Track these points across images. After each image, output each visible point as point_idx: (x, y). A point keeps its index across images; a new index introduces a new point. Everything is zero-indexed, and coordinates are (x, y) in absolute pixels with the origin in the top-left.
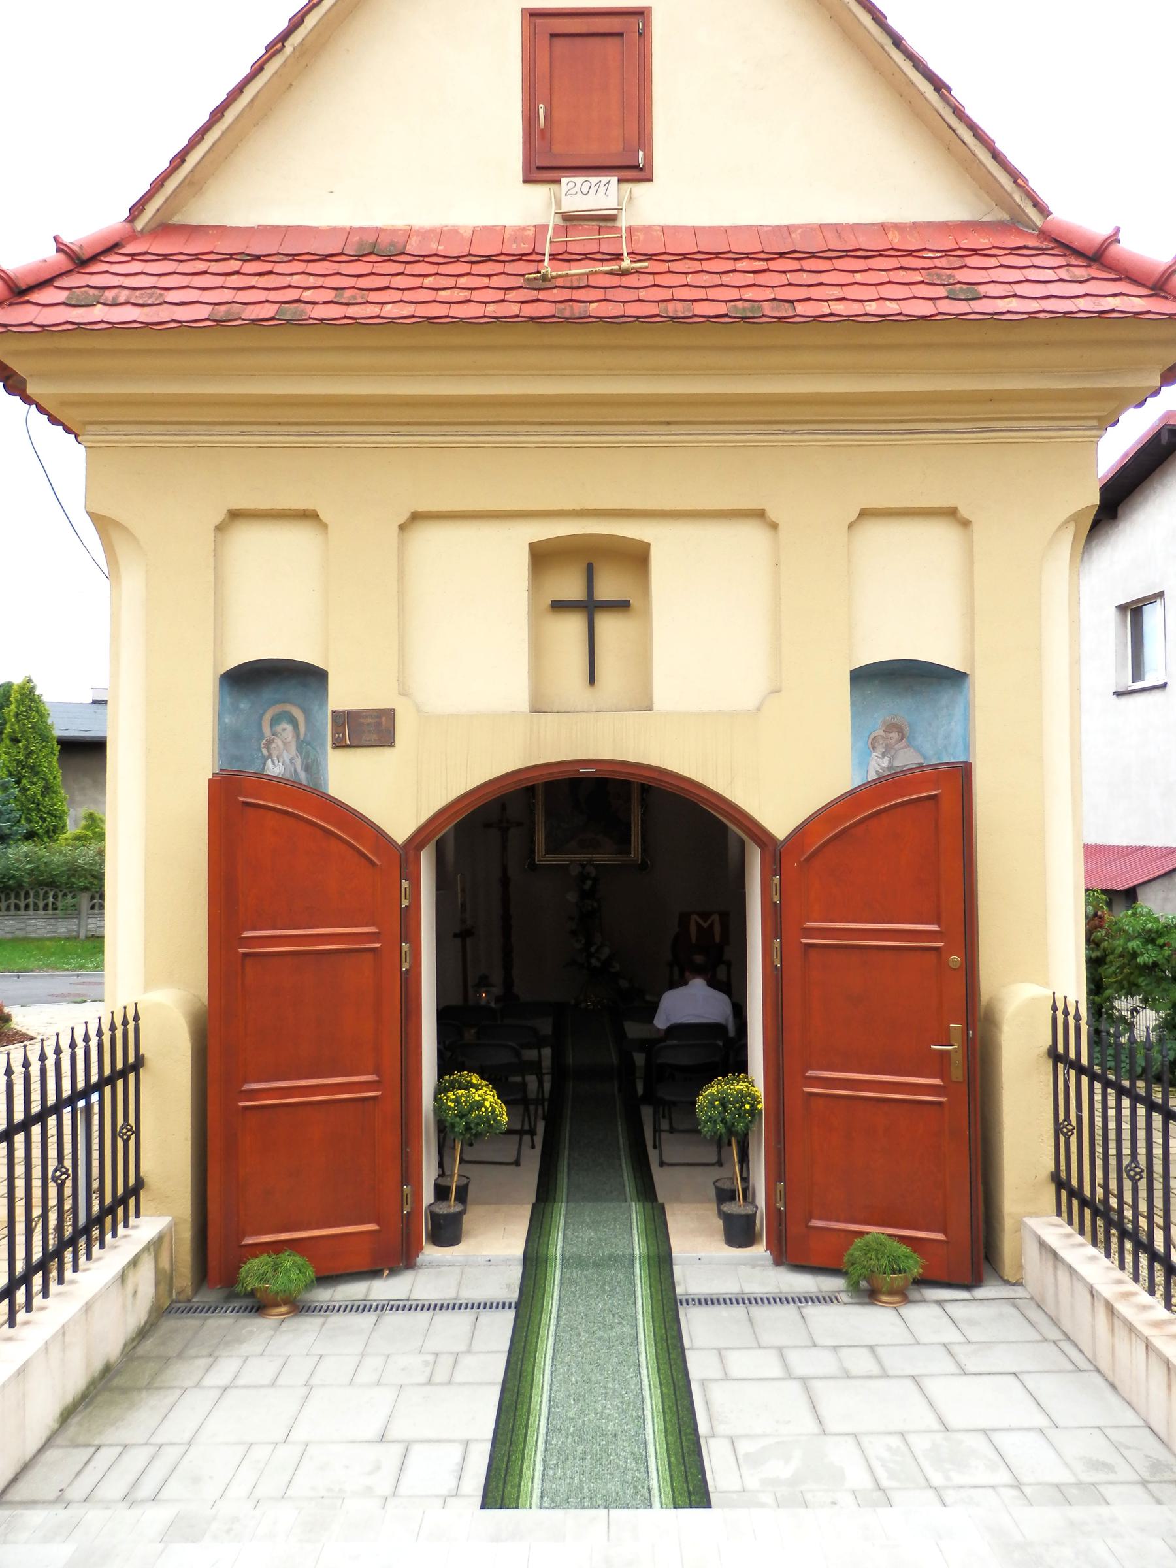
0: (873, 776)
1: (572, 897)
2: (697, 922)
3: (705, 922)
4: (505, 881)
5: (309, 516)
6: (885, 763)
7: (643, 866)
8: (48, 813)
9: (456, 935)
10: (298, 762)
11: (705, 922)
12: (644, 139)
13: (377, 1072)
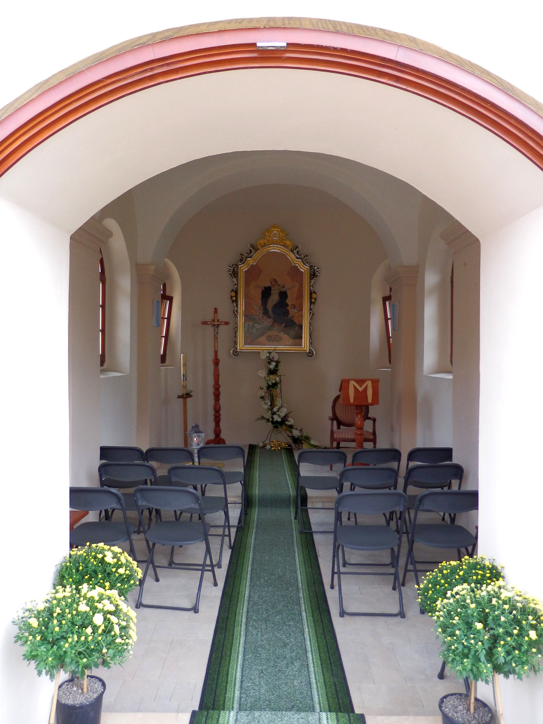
1: (263, 373)
2: (355, 387)
3: (361, 386)
4: (216, 362)
7: (310, 354)
9: (179, 397)
11: (361, 386)
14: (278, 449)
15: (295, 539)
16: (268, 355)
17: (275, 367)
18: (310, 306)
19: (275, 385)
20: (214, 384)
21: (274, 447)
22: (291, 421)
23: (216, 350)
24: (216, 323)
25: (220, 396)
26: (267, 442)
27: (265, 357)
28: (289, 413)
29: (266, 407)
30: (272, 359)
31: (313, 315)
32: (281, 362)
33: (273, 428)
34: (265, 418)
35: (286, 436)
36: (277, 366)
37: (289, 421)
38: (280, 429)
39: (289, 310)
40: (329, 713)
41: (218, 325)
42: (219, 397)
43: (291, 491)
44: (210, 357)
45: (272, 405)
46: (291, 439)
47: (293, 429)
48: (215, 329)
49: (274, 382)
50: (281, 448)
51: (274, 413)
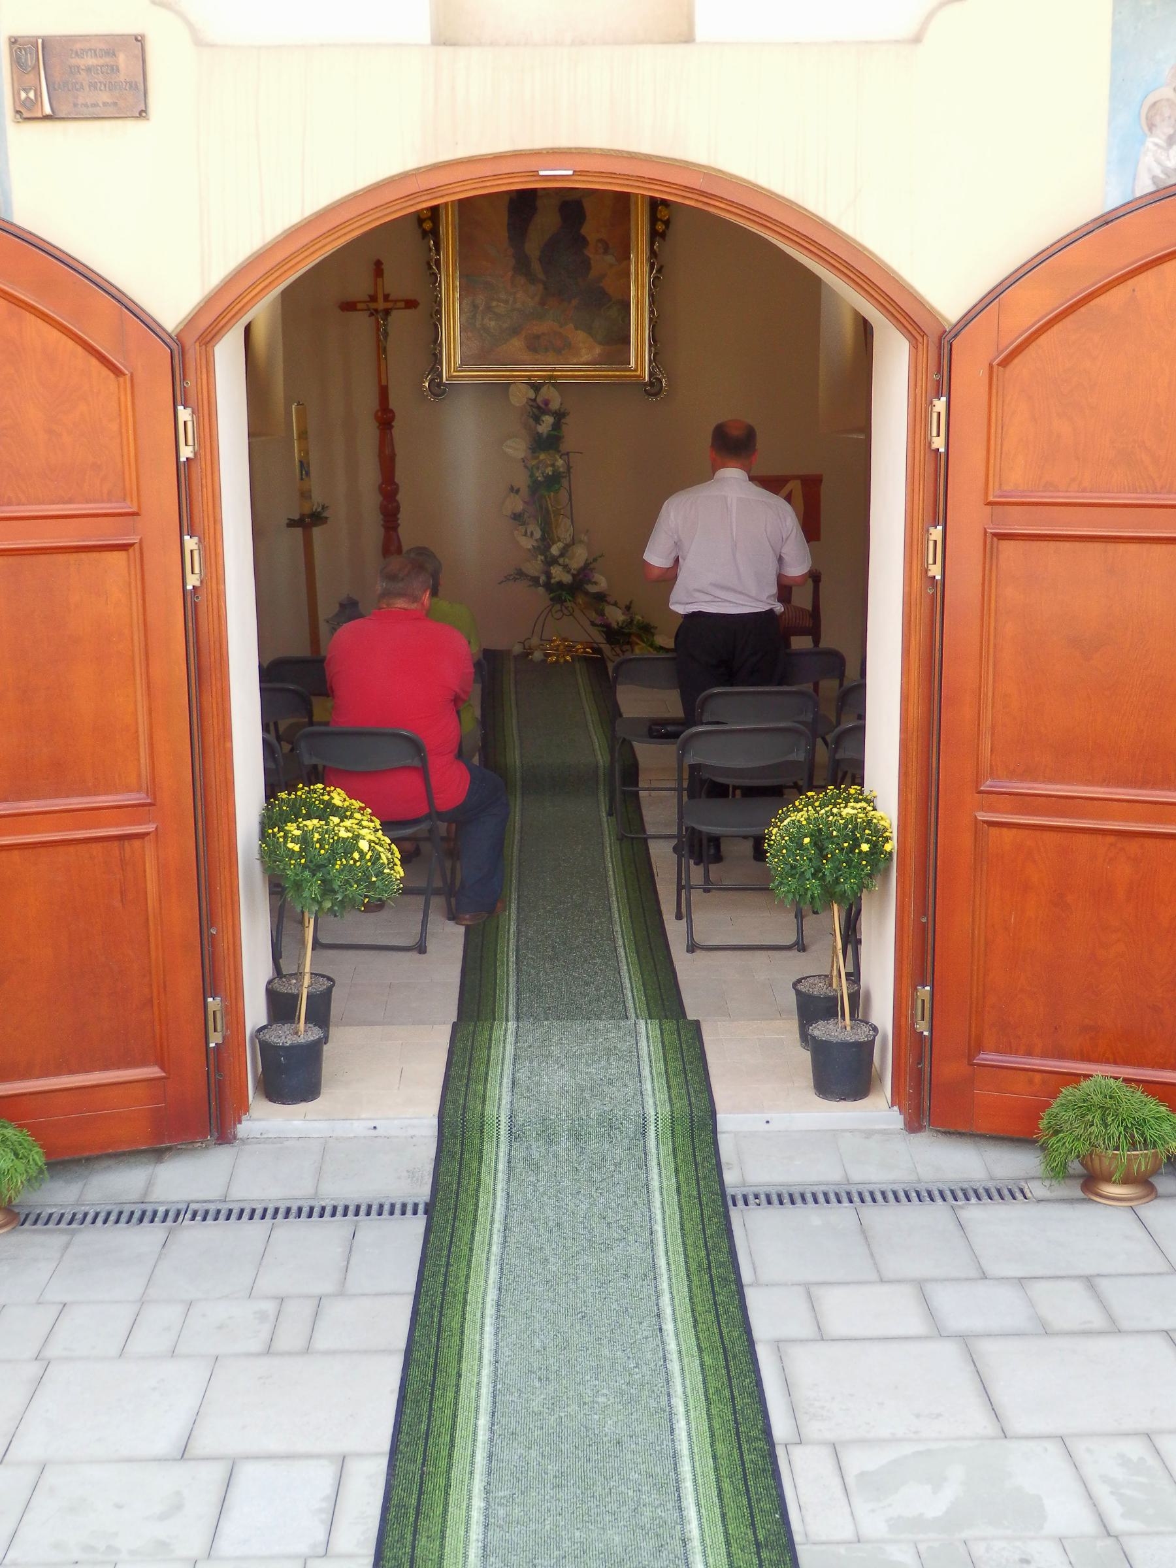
7: (653, 388)
9: (292, 523)
14: (566, 661)
15: (608, 849)
16: (532, 394)
17: (553, 429)
18: (652, 244)
19: (553, 480)
20: (380, 481)
21: (554, 654)
22: (601, 583)
23: (384, 383)
24: (381, 305)
25: (399, 516)
26: (535, 641)
27: (525, 400)
28: (595, 560)
29: (527, 543)
30: (543, 406)
31: (659, 271)
32: (568, 414)
33: (550, 603)
34: (527, 576)
35: (587, 624)
36: (557, 426)
37: (596, 583)
38: (569, 604)
39: (591, 256)
40: (649, 1021)
41: (387, 312)
42: (398, 519)
43: (600, 757)
44: (367, 403)
45: (547, 540)
46: (599, 631)
47: (604, 603)
48: (378, 322)
49: (549, 471)
50: (572, 657)
51: (552, 561)
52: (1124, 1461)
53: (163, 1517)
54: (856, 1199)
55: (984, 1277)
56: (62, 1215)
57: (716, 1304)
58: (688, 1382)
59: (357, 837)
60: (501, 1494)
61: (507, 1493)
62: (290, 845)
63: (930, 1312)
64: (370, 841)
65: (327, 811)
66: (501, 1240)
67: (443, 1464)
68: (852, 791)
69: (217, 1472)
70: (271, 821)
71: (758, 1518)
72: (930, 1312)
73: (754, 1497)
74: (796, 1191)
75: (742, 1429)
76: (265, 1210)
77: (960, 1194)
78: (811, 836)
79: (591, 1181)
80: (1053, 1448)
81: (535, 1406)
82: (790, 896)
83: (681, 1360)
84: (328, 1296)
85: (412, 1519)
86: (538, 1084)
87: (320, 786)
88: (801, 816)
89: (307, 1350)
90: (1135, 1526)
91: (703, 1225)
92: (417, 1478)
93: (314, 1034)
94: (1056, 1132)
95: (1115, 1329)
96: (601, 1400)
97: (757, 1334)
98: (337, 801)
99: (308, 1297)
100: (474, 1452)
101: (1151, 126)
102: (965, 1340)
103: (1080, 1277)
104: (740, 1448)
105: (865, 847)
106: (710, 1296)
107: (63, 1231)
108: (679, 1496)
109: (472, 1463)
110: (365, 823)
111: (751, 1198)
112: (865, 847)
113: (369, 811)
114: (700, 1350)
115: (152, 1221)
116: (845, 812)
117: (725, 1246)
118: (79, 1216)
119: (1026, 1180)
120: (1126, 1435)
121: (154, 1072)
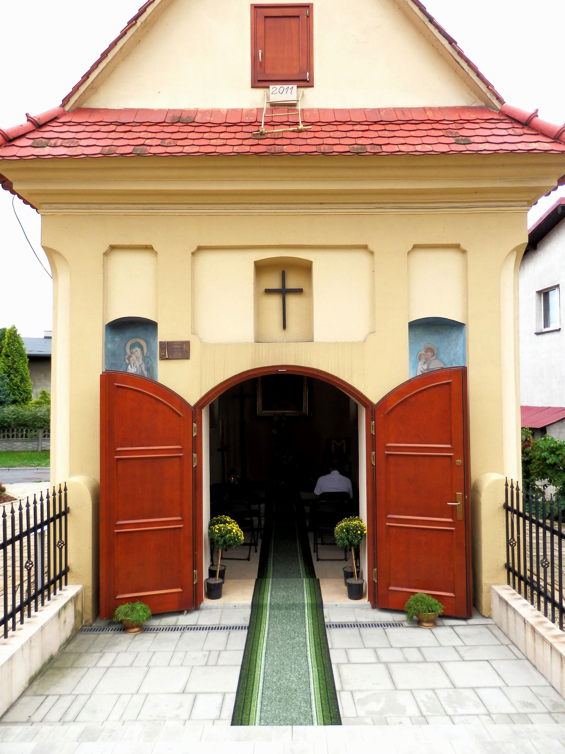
0: (419, 373)
5: (148, 248)
6: (425, 367)
8: (23, 391)
10: (143, 367)
12: (309, 67)
13: (181, 515)
52: (427, 696)
53: (178, 708)
54: (359, 626)
55: (392, 647)
56: (155, 628)
57: (322, 654)
58: (314, 674)
59: (233, 529)
60: (265, 703)
61: (267, 703)
62: (216, 531)
63: (377, 657)
64: (236, 530)
65: (225, 522)
66: (267, 636)
67: (250, 695)
68: (356, 518)
69: (191, 697)
70: (212, 524)
71: (331, 711)
72: (377, 657)
73: (330, 705)
74: (343, 624)
75: (328, 687)
76: (206, 628)
77: (386, 625)
78: (346, 529)
79: (290, 621)
80: (409, 693)
81: (274, 680)
82: (341, 545)
83: (312, 668)
84: (222, 650)
85: (242, 710)
86: (277, 595)
87: (224, 516)
88: (343, 524)
89: (216, 665)
90: (430, 714)
91: (319, 632)
92: (243, 699)
93: (220, 581)
94: (410, 608)
95: (425, 661)
96: (291, 678)
97: (332, 662)
98: (228, 520)
99: (217, 651)
100: (258, 692)
101: (420, 360)
102: (386, 664)
103: (417, 647)
104: (327, 692)
105: (359, 532)
106: (320, 651)
107: (155, 633)
108: (311, 705)
109: (258, 695)
110: (235, 525)
111: (332, 626)
112: (359, 532)
113: (236, 522)
114: (317, 666)
115: (177, 630)
116: (354, 523)
117: (324, 638)
118: (159, 629)
119: (403, 621)
120: (427, 689)
121: (179, 590)
